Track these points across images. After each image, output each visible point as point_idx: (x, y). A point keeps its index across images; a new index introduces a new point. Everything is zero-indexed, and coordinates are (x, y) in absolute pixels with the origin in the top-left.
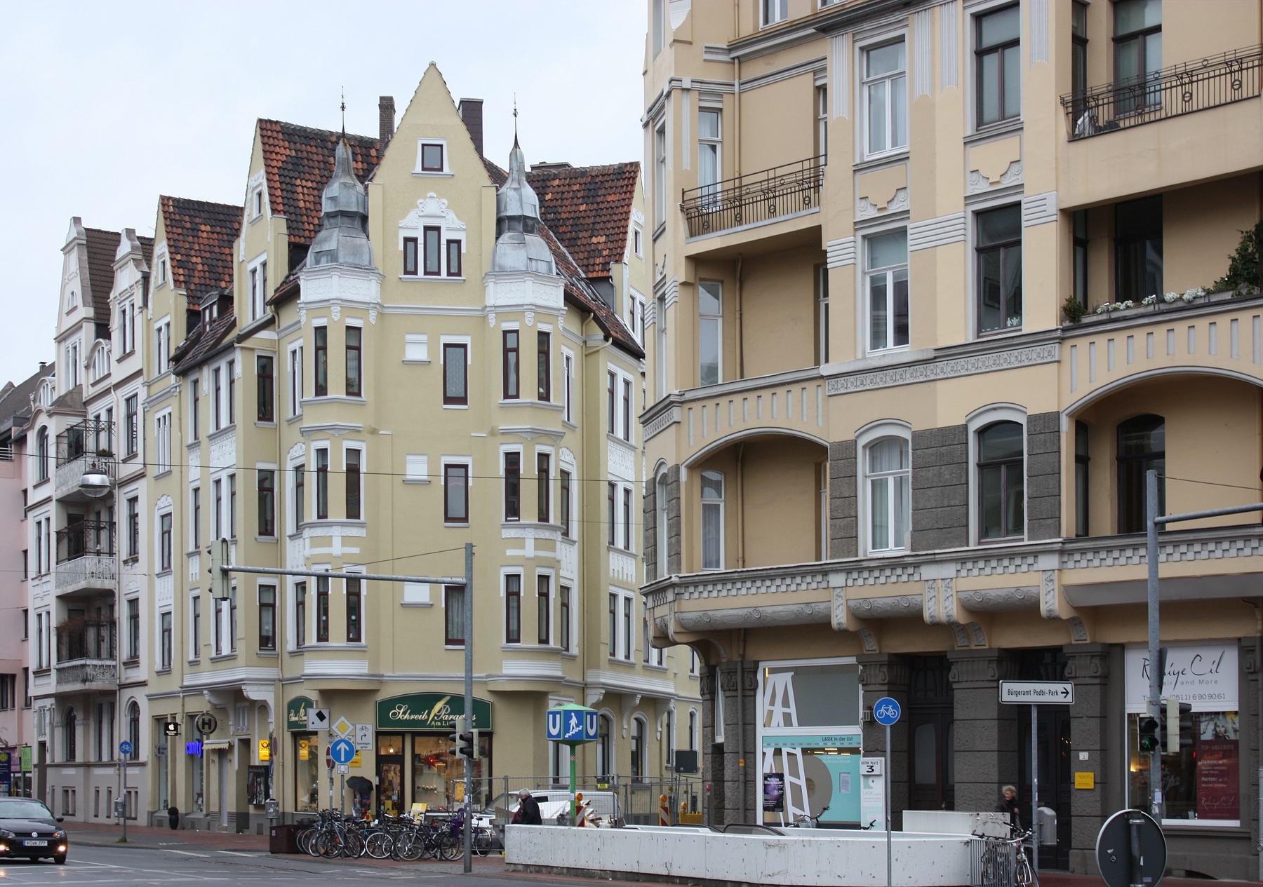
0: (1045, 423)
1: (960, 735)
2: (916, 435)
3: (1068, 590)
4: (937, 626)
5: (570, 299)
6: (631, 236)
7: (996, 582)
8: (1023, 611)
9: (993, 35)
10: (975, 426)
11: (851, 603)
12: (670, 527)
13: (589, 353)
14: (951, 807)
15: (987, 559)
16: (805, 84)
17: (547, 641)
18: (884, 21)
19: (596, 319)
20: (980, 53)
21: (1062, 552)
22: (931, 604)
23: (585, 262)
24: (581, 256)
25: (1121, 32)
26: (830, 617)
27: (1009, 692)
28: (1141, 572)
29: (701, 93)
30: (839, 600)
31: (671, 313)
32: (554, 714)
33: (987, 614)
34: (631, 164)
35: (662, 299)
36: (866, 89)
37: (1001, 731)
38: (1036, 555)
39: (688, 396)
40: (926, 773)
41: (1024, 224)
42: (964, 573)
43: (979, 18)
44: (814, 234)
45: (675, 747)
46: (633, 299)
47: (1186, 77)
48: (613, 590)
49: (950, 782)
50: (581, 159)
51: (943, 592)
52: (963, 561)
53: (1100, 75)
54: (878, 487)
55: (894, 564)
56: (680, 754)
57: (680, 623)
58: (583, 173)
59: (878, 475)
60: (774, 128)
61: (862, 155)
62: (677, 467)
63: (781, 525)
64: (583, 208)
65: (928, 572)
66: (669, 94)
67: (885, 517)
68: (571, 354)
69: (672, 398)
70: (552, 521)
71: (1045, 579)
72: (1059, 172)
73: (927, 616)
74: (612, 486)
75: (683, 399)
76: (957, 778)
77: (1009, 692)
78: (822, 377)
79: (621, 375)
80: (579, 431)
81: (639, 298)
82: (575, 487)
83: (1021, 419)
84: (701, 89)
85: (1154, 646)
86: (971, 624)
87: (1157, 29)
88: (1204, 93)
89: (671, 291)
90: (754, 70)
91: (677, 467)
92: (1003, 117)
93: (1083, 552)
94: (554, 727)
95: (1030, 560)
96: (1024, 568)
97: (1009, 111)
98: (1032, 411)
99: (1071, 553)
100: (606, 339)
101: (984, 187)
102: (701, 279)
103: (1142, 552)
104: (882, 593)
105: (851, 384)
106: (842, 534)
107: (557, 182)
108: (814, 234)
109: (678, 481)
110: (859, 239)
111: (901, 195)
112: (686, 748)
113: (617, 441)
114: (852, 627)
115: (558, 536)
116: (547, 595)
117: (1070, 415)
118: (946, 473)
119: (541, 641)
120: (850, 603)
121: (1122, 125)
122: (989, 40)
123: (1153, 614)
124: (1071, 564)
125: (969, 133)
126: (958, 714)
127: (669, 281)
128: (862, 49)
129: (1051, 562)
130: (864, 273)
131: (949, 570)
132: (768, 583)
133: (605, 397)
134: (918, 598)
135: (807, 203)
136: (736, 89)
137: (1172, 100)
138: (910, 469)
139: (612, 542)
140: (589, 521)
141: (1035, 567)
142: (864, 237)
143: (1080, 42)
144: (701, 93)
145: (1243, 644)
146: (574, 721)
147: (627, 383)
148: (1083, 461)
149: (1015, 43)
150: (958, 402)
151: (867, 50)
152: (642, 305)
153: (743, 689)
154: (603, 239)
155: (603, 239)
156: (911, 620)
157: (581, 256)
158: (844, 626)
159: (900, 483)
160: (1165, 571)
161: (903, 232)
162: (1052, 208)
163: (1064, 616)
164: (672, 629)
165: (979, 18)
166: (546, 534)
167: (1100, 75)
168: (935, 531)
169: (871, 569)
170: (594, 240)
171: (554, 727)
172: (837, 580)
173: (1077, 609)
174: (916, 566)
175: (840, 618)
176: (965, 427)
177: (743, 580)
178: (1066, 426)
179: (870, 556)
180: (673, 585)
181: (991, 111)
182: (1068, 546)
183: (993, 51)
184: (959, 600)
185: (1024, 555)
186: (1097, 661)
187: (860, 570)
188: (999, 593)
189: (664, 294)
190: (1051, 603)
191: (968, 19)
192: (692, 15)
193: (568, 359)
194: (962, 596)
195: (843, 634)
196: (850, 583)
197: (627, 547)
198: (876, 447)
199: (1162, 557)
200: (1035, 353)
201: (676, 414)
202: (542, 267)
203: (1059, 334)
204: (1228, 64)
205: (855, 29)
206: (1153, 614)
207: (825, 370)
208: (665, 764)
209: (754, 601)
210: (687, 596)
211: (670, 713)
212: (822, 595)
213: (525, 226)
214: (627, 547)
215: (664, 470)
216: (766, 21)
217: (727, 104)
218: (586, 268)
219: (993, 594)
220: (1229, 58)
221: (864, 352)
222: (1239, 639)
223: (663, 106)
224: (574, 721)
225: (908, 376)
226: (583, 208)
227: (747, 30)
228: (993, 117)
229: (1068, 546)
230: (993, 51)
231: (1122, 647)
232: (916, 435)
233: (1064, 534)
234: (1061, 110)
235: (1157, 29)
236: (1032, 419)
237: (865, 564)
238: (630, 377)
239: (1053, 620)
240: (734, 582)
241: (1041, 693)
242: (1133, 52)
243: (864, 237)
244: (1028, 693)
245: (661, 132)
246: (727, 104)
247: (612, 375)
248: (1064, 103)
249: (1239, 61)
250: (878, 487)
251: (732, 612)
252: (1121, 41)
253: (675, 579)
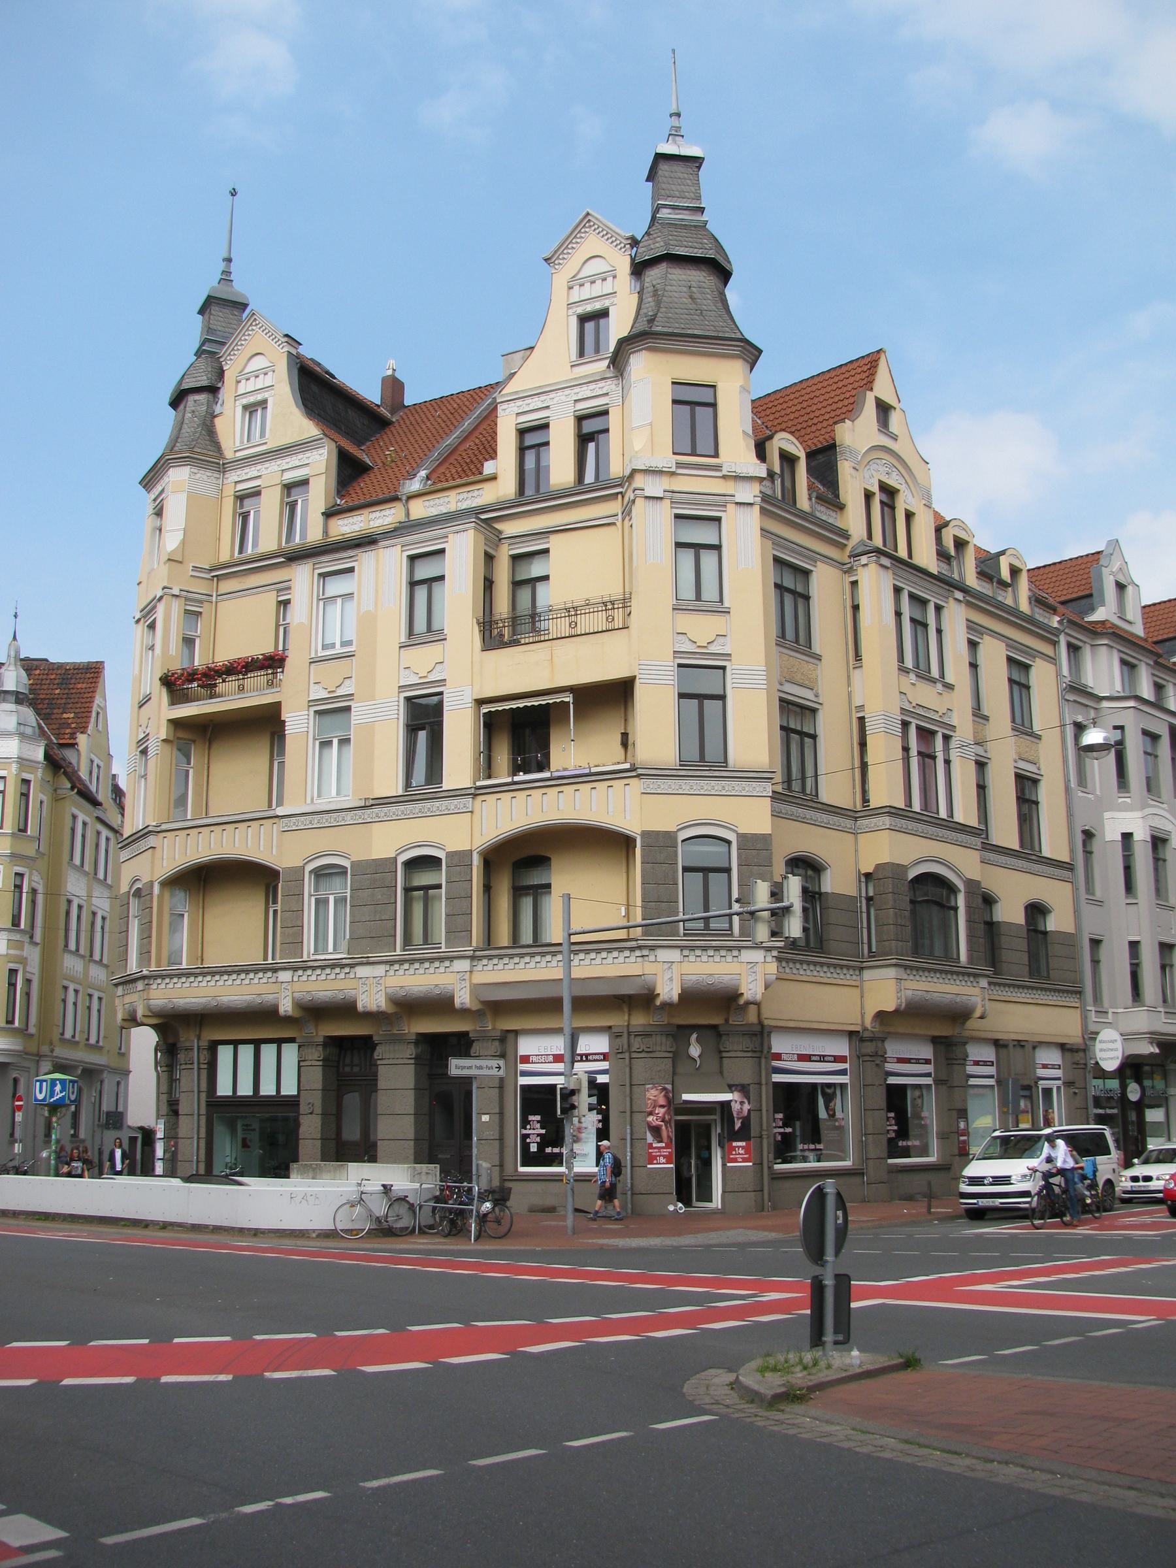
0: (460, 859)
1: (383, 1101)
2: (353, 864)
3: (475, 988)
4: (369, 1016)
5: (47, 756)
6: (94, 714)
7: (419, 980)
8: (441, 1005)
9: (424, 571)
10: (402, 859)
11: (389, 990)
12: (141, 931)
13: (57, 799)
14: (373, 1159)
15: (412, 961)
16: (270, 600)
17: (12, 1022)
18: (338, 556)
19: (65, 773)
20: (413, 584)
21: (473, 958)
22: (364, 996)
23: (57, 731)
24: (54, 726)
25: (518, 578)
26: (453, 997)
27: (457, 1067)
28: (557, 973)
29: (187, 599)
30: (285, 993)
31: (152, 763)
32: (41, 1081)
33: (410, 1006)
34: (495, 452)
35: (144, 752)
36: (321, 603)
37: (417, 1100)
38: (451, 959)
39: (164, 827)
40: (351, 1133)
41: (445, 709)
42: (392, 973)
43: (412, 559)
44: (277, 706)
45: (105, 1108)
46: (92, 761)
47: (572, 611)
48: (66, 983)
49: (372, 1138)
50: (56, 656)
51: (373, 987)
52: (391, 963)
53: (502, 606)
54: (321, 903)
55: (335, 965)
56: (108, 1114)
57: (149, 1008)
58: (61, 666)
59: (322, 893)
60: (240, 630)
61: (316, 652)
62: (152, 883)
63: (235, 929)
64: (57, 691)
65: (362, 971)
66: (161, 598)
67: (325, 928)
68: (45, 798)
69: (150, 828)
70: (22, 926)
71: (459, 980)
72: (473, 675)
73: (360, 1007)
74: (69, 902)
75: (159, 829)
76: (380, 1136)
77: (457, 1067)
78: (277, 817)
79: (81, 817)
80: (46, 858)
81: (96, 761)
82: (40, 899)
83: (441, 855)
84: (185, 596)
85: (567, 1031)
86: (395, 1013)
87: (546, 578)
88: (586, 623)
89: (154, 747)
90: (227, 586)
91: (152, 883)
92: (429, 629)
93: (490, 958)
94: (41, 1092)
95: (447, 963)
96: (442, 970)
97: (436, 626)
98: (451, 848)
99: (480, 958)
100: (72, 788)
101: (415, 680)
102: (178, 738)
103: (560, 957)
104: (323, 987)
105: (302, 822)
106: (290, 940)
107: (38, 672)
108: (277, 706)
109: (151, 894)
110: (312, 713)
111: (347, 682)
112: (113, 1109)
113: (75, 867)
114: (297, 1014)
115: (26, 939)
116: (15, 985)
117: (480, 853)
118: (379, 895)
119: (8, 1022)
120: (685, 977)
121: (523, 641)
122: (420, 575)
123: (567, 1006)
124: (480, 968)
125: (403, 640)
126: (382, 1084)
127: (152, 739)
128: (320, 575)
129: (465, 965)
130: (315, 739)
131: (380, 970)
132: (226, 977)
133: (68, 831)
134: (353, 992)
135: (270, 684)
136: (214, 599)
137: (559, 626)
138: (349, 890)
139: (66, 946)
140: (48, 929)
141: (451, 969)
142: (316, 712)
143: (489, 584)
144: (187, 599)
145: (614, 1030)
146: (58, 1088)
147: (85, 824)
148: (487, 888)
149: (441, 578)
150: (390, 840)
151: (324, 576)
152: (99, 767)
153: (199, 1063)
154: (72, 715)
155: (72, 715)
156: (346, 1010)
157: (54, 726)
158: (468, 1005)
159: (340, 901)
160: (577, 973)
161: (348, 709)
162: (468, 698)
163: (474, 1008)
164: (140, 1013)
165: (412, 559)
166: (17, 937)
167: (502, 606)
168: (369, 940)
169: (314, 968)
170: (65, 716)
171: (41, 1092)
172: (285, 976)
173: (484, 1003)
174: (352, 966)
175: (286, 1007)
176: (395, 859)
177: (204, 975)
178: (476, 860)
179: (312, 958)
180: (144, 978)
181: (420, 625)
182: (478, 953)
183: (423, 584)
184: (386, 994)
185: (441, 960)
186: (497, 1043)
187: (305, 969)
188: (421, 988)
189: (147, 748)
190: (463, 998)
191: (405, 560)
192: (183, 542)
193: (41, 802)
194: (390, 991)
195: (288, 1020)
196: (296, 979)
197: (77, 950)
198: (321, 874)
199: (575, 962)
200: (453, 804)
201: (152, 841)
202: (29, 731)
203: (473, 791)
204: (605, 604)
205: (315, 560)
206: (567, 1006)
207: (280, 811)
208: (96, 1122)
209: (211, 992)
210: (154, 986)
211: (102, 1082)
212: (274, 988)
213: (17, 698)
214: (77, 950)
215: (138, 885)
216: (241, 552)
217: (205, 609)
218: (57, 736)
219: (416, 989)
220: (605, 600)
221: (312, 799)
222: (610, 1027)
223: (155, 607)
224: (58, 1088)
225: (349, 817)
226: (57, 691)
227: (225, 557)
228: (422, 631)
229: (478, 953)
230: (423, 584)
231: (516, 1033)
232: (353, 864)
233: (474, 944)
234: (476, 628)
235: (546, 578)
236: (450, 855)
237: (310, 964)
238: (88, 819)
239: (465, 1012)
240: (196, 975)
241: (480, 1068)
242: (524, 594)
243: (316, 712)
244: (470, 1067)
245: (152, 626)
246: (205, 609)
247: (74, 817)
248: (479, 623)
249: (613, 603)
250: (321, 903)
251: (193, 1000)
252: (516, 584)
253: (145, 972)
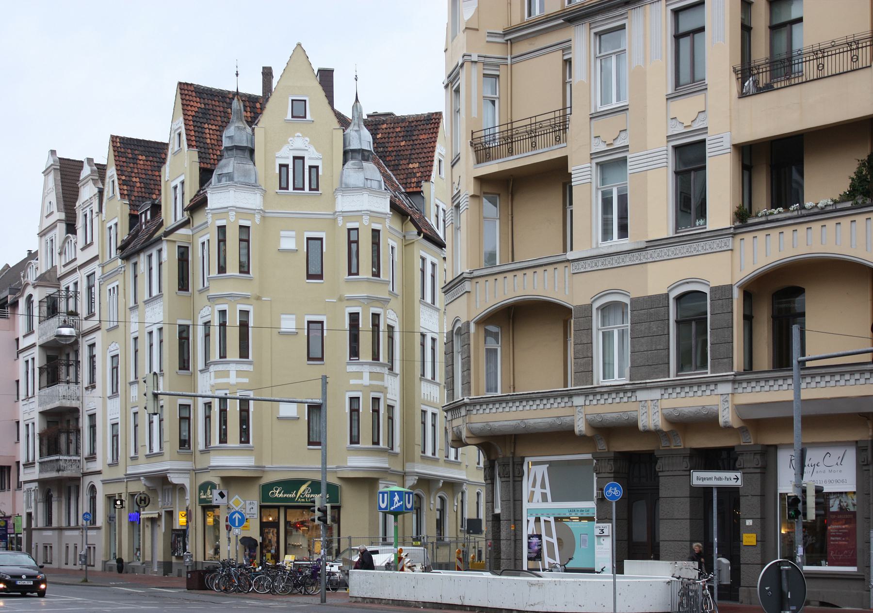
0: (723, 293)
1: (664, 508)
2: (633, 301)
3: (738, 408)
4: (648, 433)
5: (394, 206)
6: (436, 163)
7: (689, 402)
8: (707, 422)
9: (686, 24)
10: (674, 294)
11: (588, 417)
12: (463, 364)
13: (407, 244)
14: (657, 558)
15: (682, 386)
16: (557, 58)
17: (378, 443)
18: (611, 15)
19: (412, 220)
20: (678, 37)
21: (734, 382)
22: (644, 417)
23: (405, 181)
24: (402, 177)
25: (775, 22)
26: (573, 426)
27: (698, 478)
28: (789, 396)
29: (484, 64)
30: (580, 415)
31: (463, 216)
32: (383, 493)
33: (682, 424)
34: (436, 113)
35: (458, 207)
36: (598, 62)
37: (692, 505)
38: (716, 383)
39: (476, 274)
40: (640, 534)
41: (708, 155)
42: (666, 396)
43: (676, 12)
44: (563, 162)
45: (466, 516)
46: (438, 206)
47: (820, 53)
48: (424, 408)
49: (657, 540)
50: (402, 110)
51: (652, 409)
52: (666, 388)
53: (760, 52)
54: (607, 336)
55: (618, 390)
56: (470, 521)
57: (470, 430)
58: (403, 119)
59: (607, 328)
60: (535, 88)
61: (596, 107)
62: (468, 323)
63: (540, 363)
64: (403, 143)
65: (641, 395)
66: (462, 65)
67: (611, 357)
68: (395, 244)
69: (464, 275)
70: (381, 360)
71: (722, 400)
72: (732, 119)
73: (641, 426)
74: (423, 336)
75: (472, 276)
76: (662, 537)
77: (698, 478)
78: (568, 261)
79: (429, 259)
80: (400, 298)
81: (442, 206)
82: (397, 337)
83: (706, 290)
84: (485, 61)
85: (798, 446)
86: (671, 431)
87: (800, 20)
88: (832, 64)
89: (464, 201)
90: (521, 48)
91: (468, 323)
92: (693, 81)
93: (749, 381)
94: (383, 502)
95: (712, 387)
96: (708, 392)
97: (698, 77)
98: (714, 284)
99: (740, 382)
100: (419, 234)
101: (680, 129)
102: (484, 193)
103: (790, 381)
104: (610, 410)
105: (588, 265)
106: (582, 369)
107: (385, 126)
108: (563, 162)
109: (468, 332)
110: (594, 165)
111: (623, 135)
112: (474, 517)
113: (426, 305)
114: (589, 434)
115: (386, 370)
116: (378, 411)
117: (740, 287)
118: (654, 327)
119: (374, 443)
121: (775, 86)
122: (684, 27)
123: (797, 424)
124: (740, 390)
125: (670, 92)
126: (662, 493)
127: (462, 194)
128: (596, 34)
129: (726, 388)
130: (597, 189)
131: (656, 394)
132: (531, 403)
133: (418, 274)
134: (635, 414)
135: (558, 140)
136: (509, 61)
137: (810, 69)
138: (629, 324)
139: (423, 375)
140: (407, 360)
141: (716, 392)
142: (597, 164)
143: (746, 29)
144: (484, 64)
145: (859, 445)
146: (396, 498)
147: (433, 265)
148: (748, 319)
149: (702, 29)
150: (662, 278)
151: (599, 34)
152: (444, 211)
153: (514, 476)
154: (417, 165)
155: (417, 165)
156: (630, 428)
157: (402, 177)
158: (584, 433)
159: (622, 334)
160: (806, 395)
161: (624, 160)
162: (727, 144)
163: (736, 426)
164: (464, 435)
165: (676, 12)
166: (378, 369)
167: (760, 52)
168: (646, 367)
169: (602, 393)
170: (411, 166)
171: (383, 502)
172: (578, 401)
173: (744, 421)
174: (633, 391)
175: (580, 427)
176: (667, 295)
177: (514, 401)
178: (737, 294)
179: (601, 384)
180: (465, 405)
181: (685, 77)
182: (739, 377)
183: (686, 35)
184: (663, 415)
185: (708, 384)
186: (758, 457)
187: (595, 394)
188: (690, 410)
189: (459, 203)
190: (726, 417)
191: (669, 13)
192: (478, 10)
193: (392, 248)
194: (665, 412)
195: (583, 438)
196: (588, 403)
197: (433, 378)
198: (606, 309)
199: (803, 385)
200: (716, 244)
201: (467, 286)
202: (375, 185)
203: (732, 231)
204: (849, 44)
205: (591, 20)
206: (797, 424)
207: (570, 255)
208: (459, 528)
209: (521, 415)
210: (475, 412)
211: (463, 493)
212: (568, 412)
213: (363, 156)
214: (433, 378)
215: (459, 325)
216: (530, 15)
217: (502, 72)
218: (405, 185)
219: (686, 410)
220: (849, 40)
221: (597, 243)
222: (857, 442)
223: (458, 74)
224: (396, 498)
225: (627, 260)
226: (403, 143)
227: (516, 21)
228: (687, 81)
229: (739, 377)
230: (686, 35)
231: (776, 447)
232: (633, 301)
233: (735, 369)
234: (734, 76)
235: (800, 20)
236: (714, 290)
237: (598, 390)
238: (435, 261)
239: (728, 428)
240: (507, 402)
241: (720, 479)
242: (783, 36)
243: (597, 164)
244: (711, 479)
245: (457, 91)
246: (502, 72)
247: (423, 259)
248: (735, 71)
249: (857, 42)
250: (607, 336)
251: (506, 423)
252: (775, 28)
253: (466, 400)
